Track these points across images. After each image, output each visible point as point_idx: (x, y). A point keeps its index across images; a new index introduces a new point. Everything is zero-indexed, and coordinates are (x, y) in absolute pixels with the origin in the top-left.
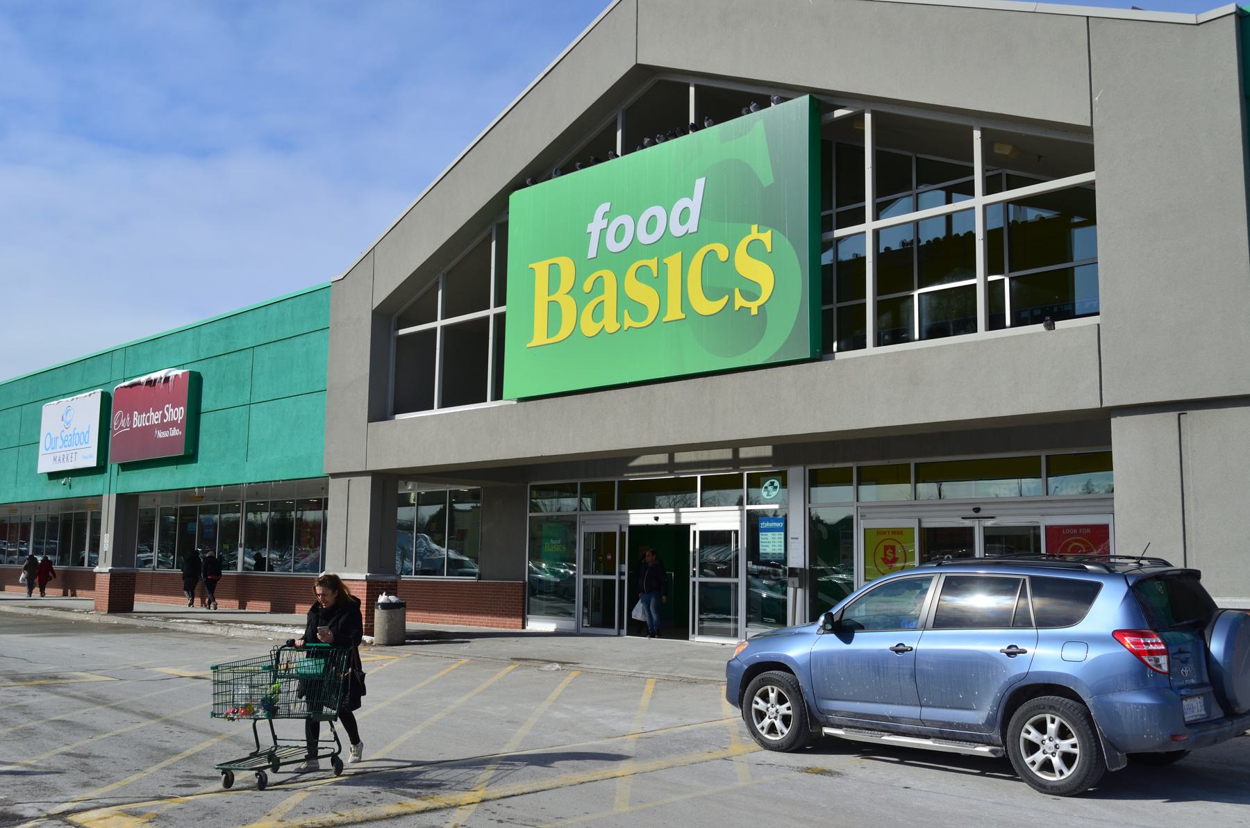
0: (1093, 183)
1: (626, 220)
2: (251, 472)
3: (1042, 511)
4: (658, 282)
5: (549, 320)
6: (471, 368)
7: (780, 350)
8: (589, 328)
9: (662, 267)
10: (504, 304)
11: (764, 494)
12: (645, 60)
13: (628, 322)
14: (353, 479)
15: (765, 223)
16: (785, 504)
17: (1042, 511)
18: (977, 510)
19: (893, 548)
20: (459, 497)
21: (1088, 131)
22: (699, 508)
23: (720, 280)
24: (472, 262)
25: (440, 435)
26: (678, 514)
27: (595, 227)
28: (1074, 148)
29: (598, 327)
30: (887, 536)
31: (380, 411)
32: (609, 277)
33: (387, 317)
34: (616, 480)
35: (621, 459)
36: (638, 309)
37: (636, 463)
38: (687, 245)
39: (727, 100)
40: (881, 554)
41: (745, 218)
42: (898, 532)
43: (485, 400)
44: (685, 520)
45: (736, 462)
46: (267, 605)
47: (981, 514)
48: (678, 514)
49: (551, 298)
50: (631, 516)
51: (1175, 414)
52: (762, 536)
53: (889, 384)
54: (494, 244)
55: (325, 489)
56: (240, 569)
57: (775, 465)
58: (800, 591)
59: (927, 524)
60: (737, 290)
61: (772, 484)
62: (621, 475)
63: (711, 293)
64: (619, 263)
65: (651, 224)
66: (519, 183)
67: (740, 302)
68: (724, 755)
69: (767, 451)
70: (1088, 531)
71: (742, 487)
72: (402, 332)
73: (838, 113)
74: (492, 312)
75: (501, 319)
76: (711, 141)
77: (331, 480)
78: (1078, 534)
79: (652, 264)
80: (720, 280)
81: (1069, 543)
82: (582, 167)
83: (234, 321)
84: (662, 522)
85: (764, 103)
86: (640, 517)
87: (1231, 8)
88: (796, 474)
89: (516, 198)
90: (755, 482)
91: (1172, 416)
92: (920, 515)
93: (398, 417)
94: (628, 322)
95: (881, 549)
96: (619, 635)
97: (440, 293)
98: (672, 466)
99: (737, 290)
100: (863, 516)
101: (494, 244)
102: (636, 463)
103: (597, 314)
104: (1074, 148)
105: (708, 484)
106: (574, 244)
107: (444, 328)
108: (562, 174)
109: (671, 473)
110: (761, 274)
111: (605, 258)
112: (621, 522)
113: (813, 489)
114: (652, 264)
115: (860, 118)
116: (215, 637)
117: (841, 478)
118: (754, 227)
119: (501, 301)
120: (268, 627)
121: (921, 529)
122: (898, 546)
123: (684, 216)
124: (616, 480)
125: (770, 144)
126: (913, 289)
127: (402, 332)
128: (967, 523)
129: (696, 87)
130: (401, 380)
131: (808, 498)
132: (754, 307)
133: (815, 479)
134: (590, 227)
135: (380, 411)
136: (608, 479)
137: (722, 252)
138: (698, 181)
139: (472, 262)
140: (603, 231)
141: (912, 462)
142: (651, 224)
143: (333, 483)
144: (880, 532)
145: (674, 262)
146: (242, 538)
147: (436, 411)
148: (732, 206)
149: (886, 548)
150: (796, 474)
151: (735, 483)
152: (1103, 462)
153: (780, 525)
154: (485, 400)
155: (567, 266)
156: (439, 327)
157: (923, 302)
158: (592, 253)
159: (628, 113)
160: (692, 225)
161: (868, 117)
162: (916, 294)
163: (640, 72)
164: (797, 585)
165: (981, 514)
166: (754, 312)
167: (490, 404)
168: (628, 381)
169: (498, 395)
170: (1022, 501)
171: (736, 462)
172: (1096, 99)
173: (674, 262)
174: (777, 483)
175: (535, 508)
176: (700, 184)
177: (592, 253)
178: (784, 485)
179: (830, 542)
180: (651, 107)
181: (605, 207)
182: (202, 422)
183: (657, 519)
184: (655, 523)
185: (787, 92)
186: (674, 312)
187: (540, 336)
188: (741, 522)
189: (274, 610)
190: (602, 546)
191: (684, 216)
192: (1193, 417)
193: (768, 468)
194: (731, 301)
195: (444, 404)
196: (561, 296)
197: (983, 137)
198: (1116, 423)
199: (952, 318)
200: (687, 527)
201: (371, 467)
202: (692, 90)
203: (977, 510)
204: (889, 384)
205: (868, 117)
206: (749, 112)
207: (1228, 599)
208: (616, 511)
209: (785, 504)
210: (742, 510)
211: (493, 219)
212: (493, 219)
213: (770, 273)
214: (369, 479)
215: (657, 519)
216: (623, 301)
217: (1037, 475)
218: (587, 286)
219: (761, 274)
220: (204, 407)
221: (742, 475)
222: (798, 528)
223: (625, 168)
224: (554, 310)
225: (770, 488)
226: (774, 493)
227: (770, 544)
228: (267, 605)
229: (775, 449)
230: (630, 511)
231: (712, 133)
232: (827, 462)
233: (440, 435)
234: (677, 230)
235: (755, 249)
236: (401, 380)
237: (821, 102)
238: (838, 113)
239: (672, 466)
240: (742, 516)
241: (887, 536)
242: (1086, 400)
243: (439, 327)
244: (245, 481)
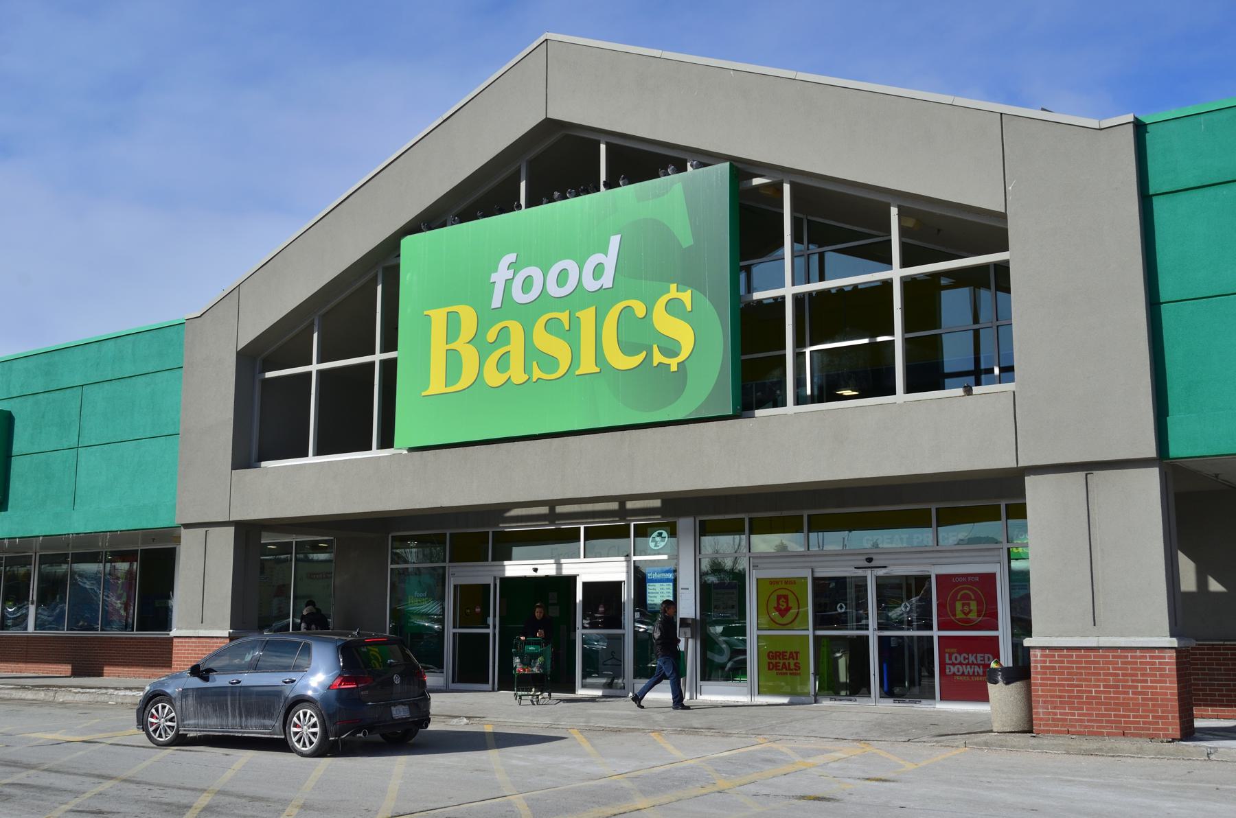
0: (1008, 261)
1: (535, 272)
2: (79, 522)
3: (934, 561)
4: (571, 335)
5: (443, 367)
6: (357, 412)
7: (701, 406)
8: (493, 378)
9: (575, 322)
10: (394, 347)
11: (652, 545)
12: (555, 114)
13: (537, 373)
14: (211, 529)
15: (684, 283)
16: (675, 557)
17: (934, 561)
18: (870, 560)
19: (786, 597)
20: (315, 547)
21: (1003, 217)
22: (582, 559)
23: (636, 336)
24: (359, 305)
25: (315, 484)
26: (559, 564)
27: (500, 276)
28: (989, 231)
29: (504, 377)
30: (779, 586)
31: (245, 458)
32: (516, 329)
33: (253, 359)
34: (491, 531)
35: (496, 512)
36: (549, 362)
37: (508, 514)
38: (601, 300)
39: (640, 161)
40: (773, 603)
41: (665, 278)
42: (788, 581)
43: (370, 448)
44: (567, 570)
45: (623, 513)
46: (67, 669)
47: (873, 564)
48: (559, 564)
49: (450, 346)
50: (507, 568)
51: (1083, 474)
52: (650, 587)
53: (810, 441)
54: (379, 288)
55: (178, 539)
56: (31, 628)
57: (664, 516)
58: (691, 642)
59: (818, 575)
60: (655, 347)
61: (660, 535)
62: (497, 526)
63: (627, 348)
64: (526, 315)
65: (562, 277)
66: (413, 227)
67: (658, 358)
68: (716, 789)
69: (657, 503)
70: (977, 579)
71: (629, 536)
72: (269, 375)
73: (756, 181)
74: (377, 357)
75: (390, 368)
76: (629, 198)
77: (184, 532)
78: (967, 583)
79: (564, 317)
80: (636, 336)
81: (957, 592)
82: (485, 216)
83: (57, 357)
84: (542, 572)
85: (681, 168)
86: (516, 568)
87: (1130, 118)
88: (686, 524)
89: (407, 243)
90: (642, 532)
91: (1080, 475)
92: (813, 565)
93: (264, 464)
94: (537, 373)
95: (774, 598)
96: (493, 690)
97: (315, 336)
98: (552, 517)
99: (655, 347)
100: (755, 567)
101: (379, 288)
102: (508, 514)
103: (503, 364)
104: (989, 231)
105: (591, 534)
106: (478, 294)
107: (320, 372)
108: (461, 222)
109: (552, 523)
110: (683, 334)
111: (509, 308)
112: (499, 574)
113: (703, 538)
114: (564, 317)
115: (777, 188)
116: (32, 703)
117: (733, 528)
118: (673, 287)
119: (390, 343)
120: (111, 691)
121: (815, 580)
122: (790, 594)
123: (598, 271)
124: (491, 531)
125: (684, 208)
126: (805, 346)
127: (269, 375)
128: (860, 573)
129: (608, 145)
130: (269, 425)
131: (698, 548)
132: (673, 363)
133: (705, 529)
134: (494, 277)
135: (245, 458)
136: (479, 532)
137: (640, 309)
138: (612, 238)
139: (359, 305)
140: (508, 282)
141: (805, 513)
142: (562, 277)
143: (184, 533)
144: (773, 581)
145: (587, 316)
146: (33, 594)
147: (311, 459)
148: (649, 263)
149: (779, 598)
150: (686, 524)
151: (622, 533)
152: (1019, 512)
153: (671, 576)
154: (370, 448)
155: (468, 315)
156: (321, 369)
157: (815, 359)
158: (496, 303)
159: (531, 164)
160: (607, 280)
161: (787, 188)
162: (808, 351)
163: (549, 126)
164: (689, 635)
165: (873, 564)
166: (674, 368)
167: (375, 453)
168: (537, 433)
169: (387, 441)
170: (782, 554)
171: (623, 513)
172: (1010, 188)
173: (587, 316)
174: (665, 534)
175: (397, 558)
176: (615, 241)
177: (496, 303)
178: (673, 534)
179: (722, 591)
180: (558, 162)
181: (511, 257)
182: (13, 466)
183: (536, 570)
184: (533, 574)
185: (706, 158)
186: (588, 365)
187: (437, 384)
188: (628, 572)
189: (75, 674)
190: (473, 600)
191: (598, 271)
192: (1098, 476)
193: (656, 519)
194: (649, 356)
195: (319, 452)
196: (460, 345)
197: (900, 214)
198: (1030, 481)
199: (872, 378)
200: (573, 579)
201: (237, 516)
202: (603, 147)
203: (870, 560)
204: (810, 441)
205: (787, 188)
206: (667, 174)
207: (1132, 639)
208: (490, 562)
209: (675, 557)
210: (628, 561)
211: (383, 264)
212: (383, 264)
213: (691, 332)
214: (232, 530)
215: (536, 570)
216: (531, 352)
217: (798, 530)
218: (491, 335)
219: (683, 334)
220: (17, 447)
221: (629, 525)
222: (688, 580)
223: (528, 221)
224: (453, 362)
225: (658, 539)
226: (662, 544)
227: (657, 594)
228: (67, 669)
229: (663, 502)
230: (506, 563)
231: (627, 193)
232: (719, 513)
233: (315, 484)
234: (590, 284)
235: (674, 308)
236: (269, 425)
237: (741, 170)
238: (756, 181)
239: (552, 517)
240: (628, 567)
241: (779, 586)
242: (1005, 461)
243: (321, 369)
244: (72, 531)
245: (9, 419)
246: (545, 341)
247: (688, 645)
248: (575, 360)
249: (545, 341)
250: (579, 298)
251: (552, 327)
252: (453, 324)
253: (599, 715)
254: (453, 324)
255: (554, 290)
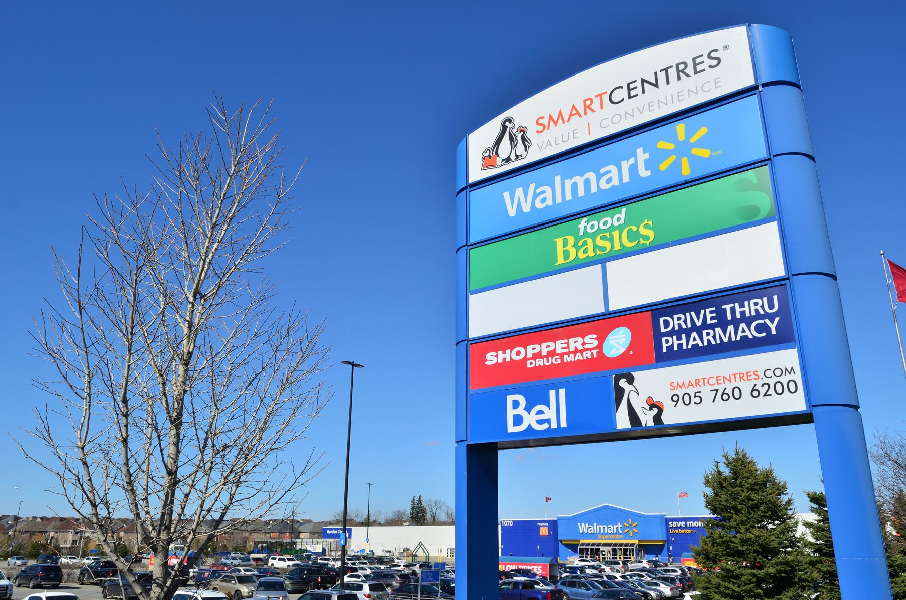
13: (598, 252)
32: (590, 241)
38: (620, 228)
64: (593, 236)
67: (642, 241)
79: (607, 235)
103: (585, 251)
114: (607, 235)
123: (618, 220)
137: (634, 228)
140: (585, 227)
145: (616, 234)
158: (581, 233)
160: (622, 222)
173: (616, 234)
177: (581, 233)
191: (618, 220)
216: (596, 247)
218: (580, 243)
245: (903, 296)
246: (599, 242)
247: (49, 563)
248: (612, 246)
249: (607, 245)
250: (612, 228)
251: (603, 238)
252: (565, 243)
253: (331, 529)
254: (565, 243)
255: (602, 227)
